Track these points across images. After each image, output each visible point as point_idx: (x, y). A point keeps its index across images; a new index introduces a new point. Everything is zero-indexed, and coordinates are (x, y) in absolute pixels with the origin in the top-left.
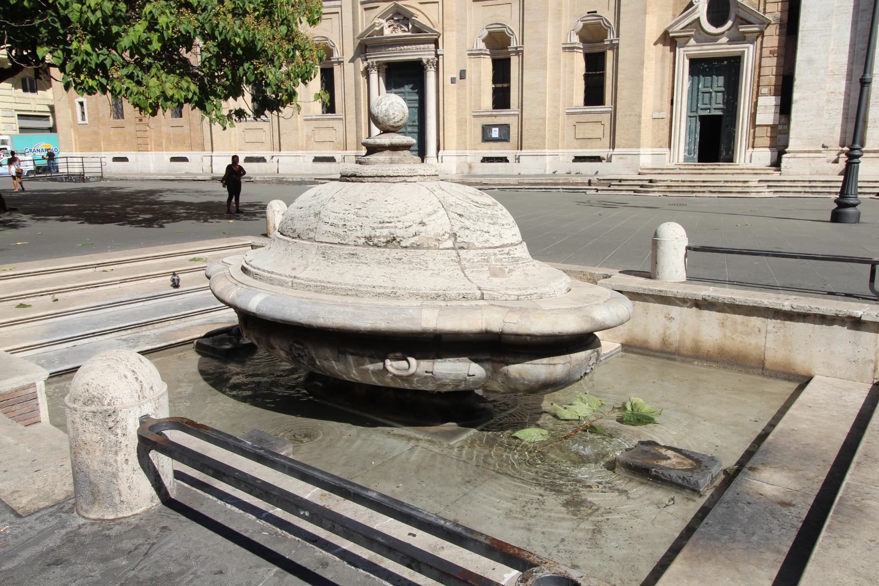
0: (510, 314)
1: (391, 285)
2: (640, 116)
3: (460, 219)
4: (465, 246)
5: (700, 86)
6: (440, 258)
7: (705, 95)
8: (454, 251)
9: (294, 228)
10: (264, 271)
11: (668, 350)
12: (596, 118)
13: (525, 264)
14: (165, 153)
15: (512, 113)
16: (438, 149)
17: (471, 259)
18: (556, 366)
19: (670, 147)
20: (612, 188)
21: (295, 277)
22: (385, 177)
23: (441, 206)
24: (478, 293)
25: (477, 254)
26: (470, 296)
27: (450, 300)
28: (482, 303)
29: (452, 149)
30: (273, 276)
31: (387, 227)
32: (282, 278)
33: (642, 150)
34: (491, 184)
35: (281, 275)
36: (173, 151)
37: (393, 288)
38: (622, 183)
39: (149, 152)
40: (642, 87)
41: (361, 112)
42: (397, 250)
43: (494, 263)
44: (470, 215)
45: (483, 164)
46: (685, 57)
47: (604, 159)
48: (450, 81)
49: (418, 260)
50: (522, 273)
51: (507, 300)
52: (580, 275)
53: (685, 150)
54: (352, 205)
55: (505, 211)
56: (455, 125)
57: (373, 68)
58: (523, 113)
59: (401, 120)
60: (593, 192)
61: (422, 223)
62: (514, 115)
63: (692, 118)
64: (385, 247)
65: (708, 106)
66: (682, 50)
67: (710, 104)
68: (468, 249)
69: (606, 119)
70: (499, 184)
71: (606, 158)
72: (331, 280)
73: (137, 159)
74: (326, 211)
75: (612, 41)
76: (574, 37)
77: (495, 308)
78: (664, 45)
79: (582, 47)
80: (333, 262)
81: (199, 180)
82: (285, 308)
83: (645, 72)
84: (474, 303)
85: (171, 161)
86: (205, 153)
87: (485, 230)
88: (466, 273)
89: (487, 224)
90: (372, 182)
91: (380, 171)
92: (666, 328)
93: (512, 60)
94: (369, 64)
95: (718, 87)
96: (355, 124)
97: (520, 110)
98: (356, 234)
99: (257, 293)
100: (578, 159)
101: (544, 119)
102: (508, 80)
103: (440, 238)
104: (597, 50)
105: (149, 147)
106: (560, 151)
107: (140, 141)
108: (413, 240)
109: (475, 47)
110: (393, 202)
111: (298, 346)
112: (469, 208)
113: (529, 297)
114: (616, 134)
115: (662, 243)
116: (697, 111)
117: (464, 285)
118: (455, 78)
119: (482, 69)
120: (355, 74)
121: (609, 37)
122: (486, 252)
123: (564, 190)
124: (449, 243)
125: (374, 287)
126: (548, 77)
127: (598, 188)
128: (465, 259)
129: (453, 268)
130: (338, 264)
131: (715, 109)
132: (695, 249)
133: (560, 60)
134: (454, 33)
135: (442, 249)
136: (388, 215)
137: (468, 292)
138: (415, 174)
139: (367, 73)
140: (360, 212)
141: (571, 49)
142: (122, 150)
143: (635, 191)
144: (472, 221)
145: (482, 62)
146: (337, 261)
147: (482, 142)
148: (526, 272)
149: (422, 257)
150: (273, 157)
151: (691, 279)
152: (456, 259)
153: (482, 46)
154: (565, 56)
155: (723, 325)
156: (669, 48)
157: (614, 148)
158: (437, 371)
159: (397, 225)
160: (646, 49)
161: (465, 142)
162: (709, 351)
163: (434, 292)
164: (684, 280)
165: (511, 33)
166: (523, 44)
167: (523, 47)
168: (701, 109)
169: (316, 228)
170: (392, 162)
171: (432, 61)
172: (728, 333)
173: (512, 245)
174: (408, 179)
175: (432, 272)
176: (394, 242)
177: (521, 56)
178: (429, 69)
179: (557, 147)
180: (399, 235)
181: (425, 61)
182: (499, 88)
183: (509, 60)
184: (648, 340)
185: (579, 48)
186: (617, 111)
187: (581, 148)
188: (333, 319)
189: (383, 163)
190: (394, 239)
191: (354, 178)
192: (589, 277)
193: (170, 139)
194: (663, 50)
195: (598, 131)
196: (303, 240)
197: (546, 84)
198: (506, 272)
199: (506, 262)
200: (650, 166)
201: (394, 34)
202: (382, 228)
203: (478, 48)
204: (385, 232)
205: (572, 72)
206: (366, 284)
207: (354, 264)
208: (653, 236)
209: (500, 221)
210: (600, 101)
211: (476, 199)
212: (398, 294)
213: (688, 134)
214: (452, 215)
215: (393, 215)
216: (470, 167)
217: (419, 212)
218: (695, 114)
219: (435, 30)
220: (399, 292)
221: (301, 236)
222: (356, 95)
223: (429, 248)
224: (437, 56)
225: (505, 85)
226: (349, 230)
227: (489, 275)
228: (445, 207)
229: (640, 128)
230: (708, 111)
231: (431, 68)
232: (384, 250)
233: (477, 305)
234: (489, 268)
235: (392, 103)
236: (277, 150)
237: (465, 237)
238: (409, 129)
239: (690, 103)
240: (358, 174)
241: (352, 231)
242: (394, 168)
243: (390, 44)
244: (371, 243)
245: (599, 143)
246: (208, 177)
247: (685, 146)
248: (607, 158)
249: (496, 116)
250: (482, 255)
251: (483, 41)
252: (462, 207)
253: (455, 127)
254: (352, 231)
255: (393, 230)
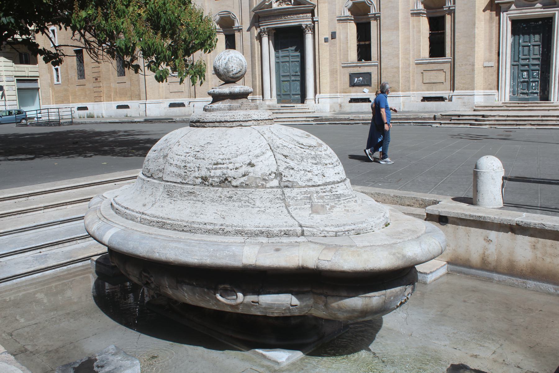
0: (325, 252)
1: (222, 221)
2: (473, 65)
3: (285, 160)
4: (290, 185)
5: (521, 41)
6: (266, 196)
7: (524, 48)
8: (279, 190)
9: (149, 168)
10: (122, 207)
11: (487, 268)
12: (439, 67)
13: (347, 200)
14: (113, 102)
15: (373, 64)
16: (316, 93)
17: (294, 197)
18: (371, 299)
19: (498, 89)
20: (452, 122)
21: (143, 213)
22: (223, 122)
23: (269, 148)
24: (299, 230)
25: (301, 192)
26: (291, 232)
27: (273, 236)
28: (302, 239)
29: (326, 93)
30: (127, 211)
31: (220, 168)
32: (134, 213)
33: (476, 92)
34: (356, 120)
35: (133, 211)
36: (118, 101)
37: (222, 225)
38: (460, 118)
39: (102, 103)
40: (475, 42)
41: (256, 66)
42: (228, 189)
43: (316, 200)
44: (295, 156)
45: (351, 104)
46: (508, 19)
47: (446, 99)
48: (324, 41)
49: (247, 198)
50: (343, 210)
51: (326, 236)
52: (413, 201)
53: (510, 91)
54: (193, 148)
55: (330, 151)
56: (328, 74)
57: (265, 33)
58: (382, 64)
59: (240, 72)
60: (438, 125)
61: (251, 165)
62: (375, 65)
63: (515, 67)
64: (218, 186)
65: (527, 57)
66: (505, 13)
67: (529, 55)
68: (292, 187)
69: (447, 67)
70: (363, 120)
71: (448, 98)
72: (170, 217)
73: (93, 107)
74: (172, 154)
75: (450, 7)
76: (419, 5)
77: (312, 245)
78: (491, 11)
79: (426, 12)
80: (175, 199)
81: (135, 122)
82: (130, 243)
83: (476, 31)
84: (293, 239)
85: (117, 108)
86: (141, 101)
87: (308, 170)
88: (290, 210)
89: (310, 164)
90: (212, 127)
91: (219, 117)
92: (486, 249)
93: (371, 23)
94: (261, 30)
95: (535, 41)
96: (251, 76)
97: (379, 62)
98: (193, 175)
99: (113, 227)
100: (425, 99)
101: (398, 68)
102: (369, 39)
103: (267, 178)
104: (438, 15)
105: (102, 99)
106: (411, 93)
107: (96, 95)
108: (242, 180)
109: (343, 14)
110: (226, 145)
111: (145, 274)
112: (295, 150)
113: (347, 233)
114: (455, 79)
115: (482, 174)
116: (518, 61)
117: (286, 222)
118: (328, 38)
119: (349, 31)
120: (251, 38)
121: (447, 4)
122: (309, 190)
123: (415, 124)
124: (275, 183)
125: (205, 224)
126: (400, 36)
127: (442, 122)
128: (289, 197)
129: (278, 205)
130: (179, 202)
131: (533, 59)
132: (510, 180)
133: (410, 22)
134: (326, 4)
135: (268, 188)
136: (222, 157)
137: (290, 229)
138: (250, 119)
139: (260, 38)
140: (199, 155)
141: (417, 14)
142: (84, 102)
143: (471, 124)
144: (296, 162)
145: (348, 26)
146: (179, 199)
147: (350, 87)
148: (347, 208)
149: (250, 196)
150: (190, 102)
151: (508, 204)
152: (281, 197)
153: (348, 13)
154: (413, 20)
155: (534, 247)
156: (495, 12)
157: (453, 90)
158: (262, 301)
159: (228, 166)
160: (477, 13)
161: (336, 87)
162: (522, 270)
163: (258, 229)
164: (502, 205)
165: (370, 3)
166: (380, 11)
167: (380, 13)
168: (522, 59)
169: (164, 169)
170: (230, 109)
171: (309, 26)
172: (539, 255)
173: (334, 183)
174: (243, 124)
175: (258, 209)
176: (226, 182)
177: (378, 20)
178: (307, 32)
179: (409, 90)
180: (230, 175)
181: (304, 26)
182: (362, 45)
183: (370, 23)
184: (470, 259)
185: (424, 14)
186: (456, 61)
187: (428, 90)
188: (166, 254)
189: (224, 110)
190: (226, 179)
191: (198, 124)
192: (421, 202)
193: (117, 92)
194: (491, 14)
195: (441, 77)
196: (155, 179)
197: (399, 41)
198: (328, 209)
199: (328, 199)
200: (483, 104)
201: (280, 7)
202: (216, 169)
203: (345, 15)
204: (218, 172)
205: (419, 32)
206: (199, 221)
207: (192, 202)
208: (474, 167)
209: (324, 161)
210: (442, 54)
211: (302, 141)
212: (225, 231)
213: (512, 79)
214: (279, 156)
215: (225, 157)
216: (341, 106)
217: (249, 154)
218: (517, 63)
219: (312, 2)
220: (227, 229)
221: (153, 175)
222: (251, 53)
223: (257, 187)
224: (314, 22)
225: (367, 43)
226: (189, 171)
227: (310, 212)
228: (272, 148)
229: (474, 74)
230: (528, 60)
231: (309, 31)
232: (217, 189)
233: (296, 242)
234: (312, 206)
235: (232, 57)
236: (193, 97)
237: (289, 176)
238: (293, 78)
239: (513, 55)
240: (201, 120)
241: (191, 171)
242: (231, 114)
243: (277, 14)
244: (207, 183)
245: (441, 85)
246: (142, 120)
247: (510, 88)
248: (449, 98)
249: (360, 67)
250: (305, 192)
251: (349, 10)
252: (288, 149)
253: (328, 76)
254: (191, 171)
255: (225, 171)
